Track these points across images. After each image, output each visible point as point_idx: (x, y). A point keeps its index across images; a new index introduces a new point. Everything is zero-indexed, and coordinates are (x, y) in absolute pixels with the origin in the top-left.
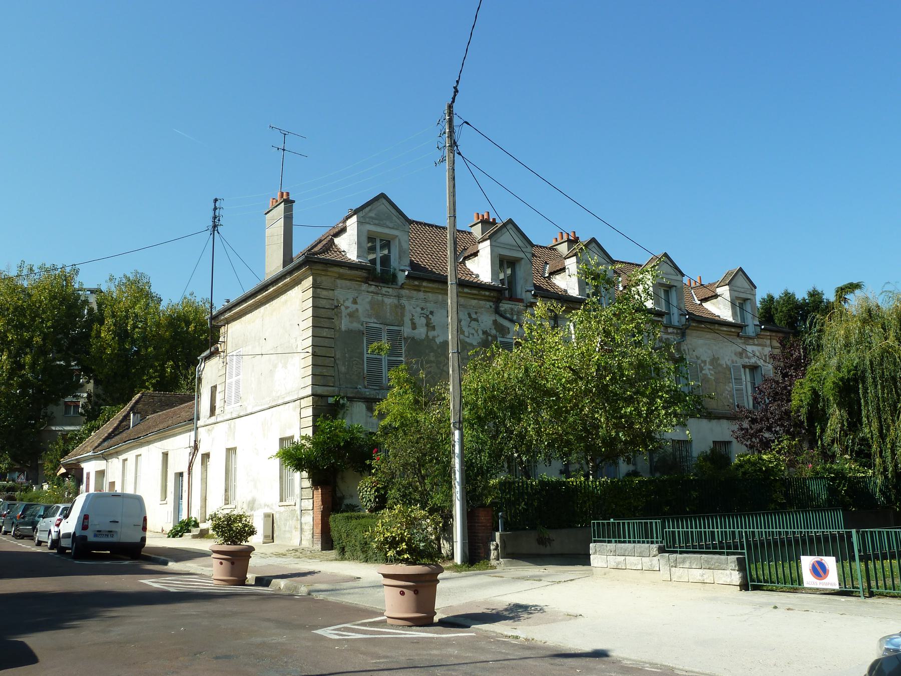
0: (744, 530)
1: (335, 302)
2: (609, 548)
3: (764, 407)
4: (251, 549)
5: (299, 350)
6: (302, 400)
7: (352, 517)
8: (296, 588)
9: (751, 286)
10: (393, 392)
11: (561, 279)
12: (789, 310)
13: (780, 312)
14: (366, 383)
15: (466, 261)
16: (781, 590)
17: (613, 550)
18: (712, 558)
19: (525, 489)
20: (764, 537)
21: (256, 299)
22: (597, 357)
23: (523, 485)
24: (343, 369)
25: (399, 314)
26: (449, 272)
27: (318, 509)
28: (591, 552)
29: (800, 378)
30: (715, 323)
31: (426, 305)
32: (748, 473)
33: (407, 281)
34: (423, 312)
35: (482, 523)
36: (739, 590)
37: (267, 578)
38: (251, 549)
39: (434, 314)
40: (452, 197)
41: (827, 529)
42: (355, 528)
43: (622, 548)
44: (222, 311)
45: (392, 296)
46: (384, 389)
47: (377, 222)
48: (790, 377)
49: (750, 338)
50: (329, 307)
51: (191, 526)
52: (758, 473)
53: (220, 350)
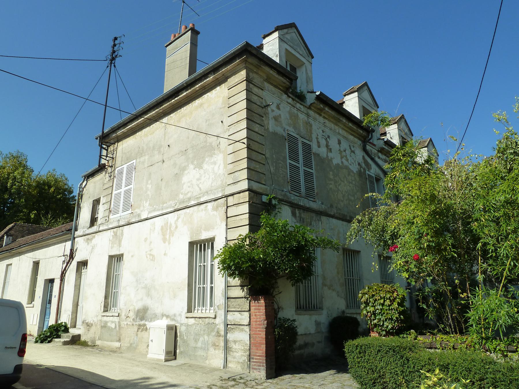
44: (115, 127)
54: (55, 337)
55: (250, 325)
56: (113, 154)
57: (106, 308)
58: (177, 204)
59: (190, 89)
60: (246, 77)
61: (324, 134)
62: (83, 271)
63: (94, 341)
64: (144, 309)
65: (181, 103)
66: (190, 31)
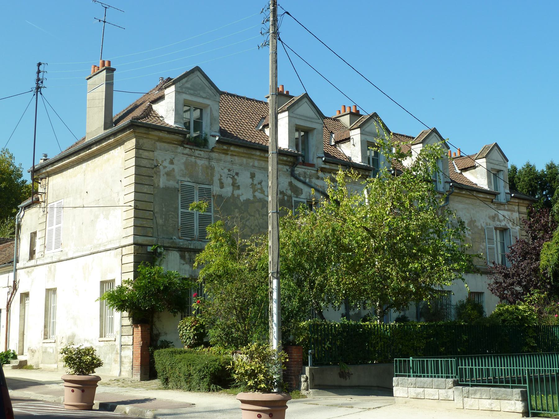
0: (527, 368)
1: (155, 161)
2: (410, 381)
3: (516, 264)
4: (98, 379)
5: (121, 203)
6: (124, 248)
7: (176, 352)
8: (141, 412)
9: (504, 159)
10: (210, 244)
11: (345, 148)
12: (530, 180)
13: (523, 181)
14: (180, 235)
15: (265, 129)
16: (555, 417)
17: (413, 383)
18: (499, 391)
19: (330, 330)
20: (521, 374)
21: (79, 156)
22: (389, 219)
23: (328, 327)
24: (160, 221)
25: (209, 174)
26: (270, 144)
27: (138, 344)
28: (394, 384)
29: (548, 241)
30: (473, 190)
31: (232, 167)
32: (507, 321)
33: (217, 145)
34: (229, 173)
35: (294, 358)
36: (522, 416)
37: (111, 404)
38: (98, 379)
39: (239, 175)
40: (274, 78)
41: (553, 367)
42: (180, 362)
43: (421, 382)
45: (203, 158)
46: (195, 240)
47: (192, 92)
48: (538, 239)
49: (501, 204)
50: (149, 166)
51: (10, 358)
52: (515, 321)
53: (40, 200)
54: (5, 362)
55: (133, 345)
56: (45, 189)
57: (46, 336)
58: (93, 248)
59: (99, 145)
60: (135, 146)
61: (231, 173)
62: (26, 302)
63: (37, 365)
64: (72, 336)
65: (95, 153)
66: (105, 71)
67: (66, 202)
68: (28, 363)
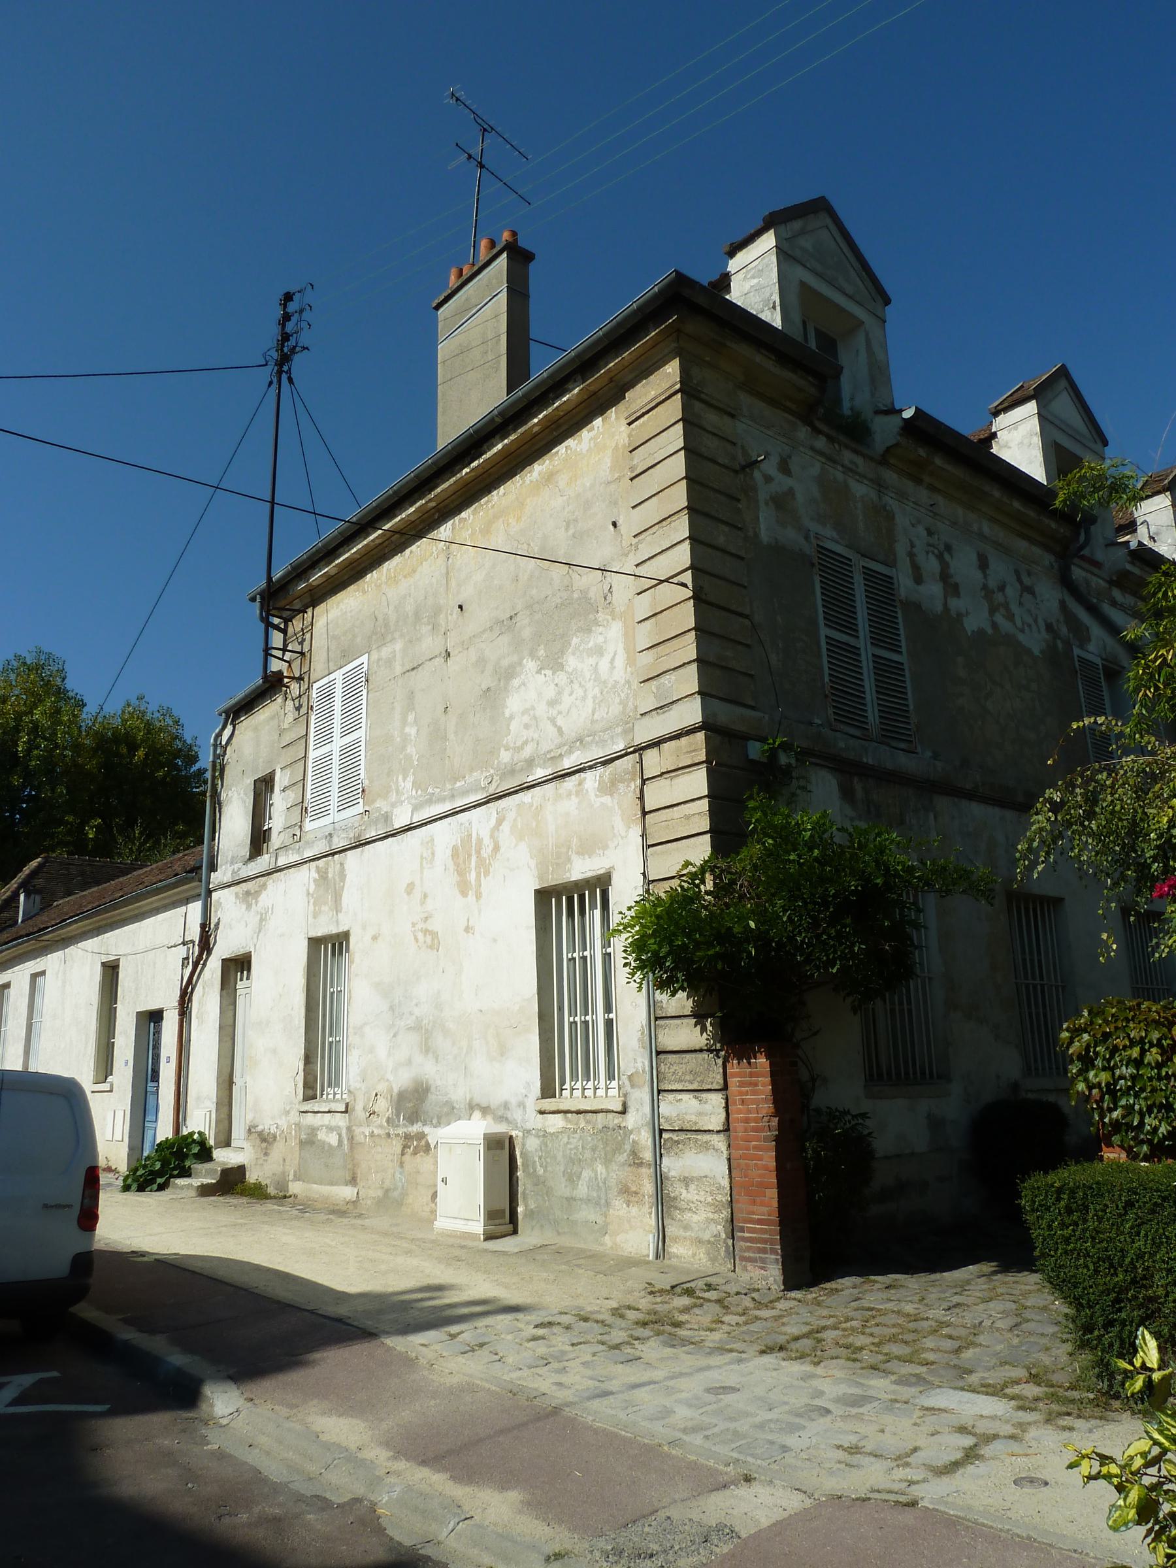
51: (191, 1157)
54: (176, 1172)
56: (301, 643)
57: (311, 1091)
59: (515, 430)
62: (240, 985)
63: (282, 1185)
64: (416, 1090)
67: (379, 660)
68: (247, 1174)
